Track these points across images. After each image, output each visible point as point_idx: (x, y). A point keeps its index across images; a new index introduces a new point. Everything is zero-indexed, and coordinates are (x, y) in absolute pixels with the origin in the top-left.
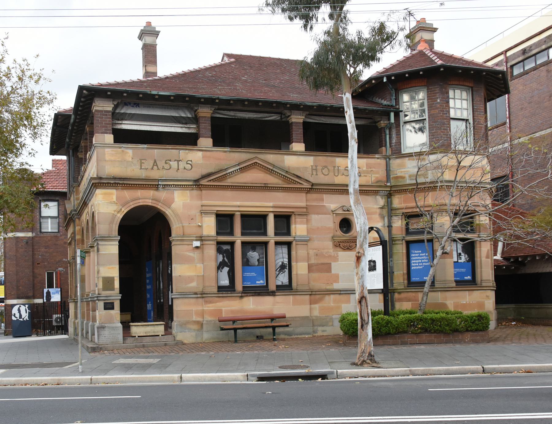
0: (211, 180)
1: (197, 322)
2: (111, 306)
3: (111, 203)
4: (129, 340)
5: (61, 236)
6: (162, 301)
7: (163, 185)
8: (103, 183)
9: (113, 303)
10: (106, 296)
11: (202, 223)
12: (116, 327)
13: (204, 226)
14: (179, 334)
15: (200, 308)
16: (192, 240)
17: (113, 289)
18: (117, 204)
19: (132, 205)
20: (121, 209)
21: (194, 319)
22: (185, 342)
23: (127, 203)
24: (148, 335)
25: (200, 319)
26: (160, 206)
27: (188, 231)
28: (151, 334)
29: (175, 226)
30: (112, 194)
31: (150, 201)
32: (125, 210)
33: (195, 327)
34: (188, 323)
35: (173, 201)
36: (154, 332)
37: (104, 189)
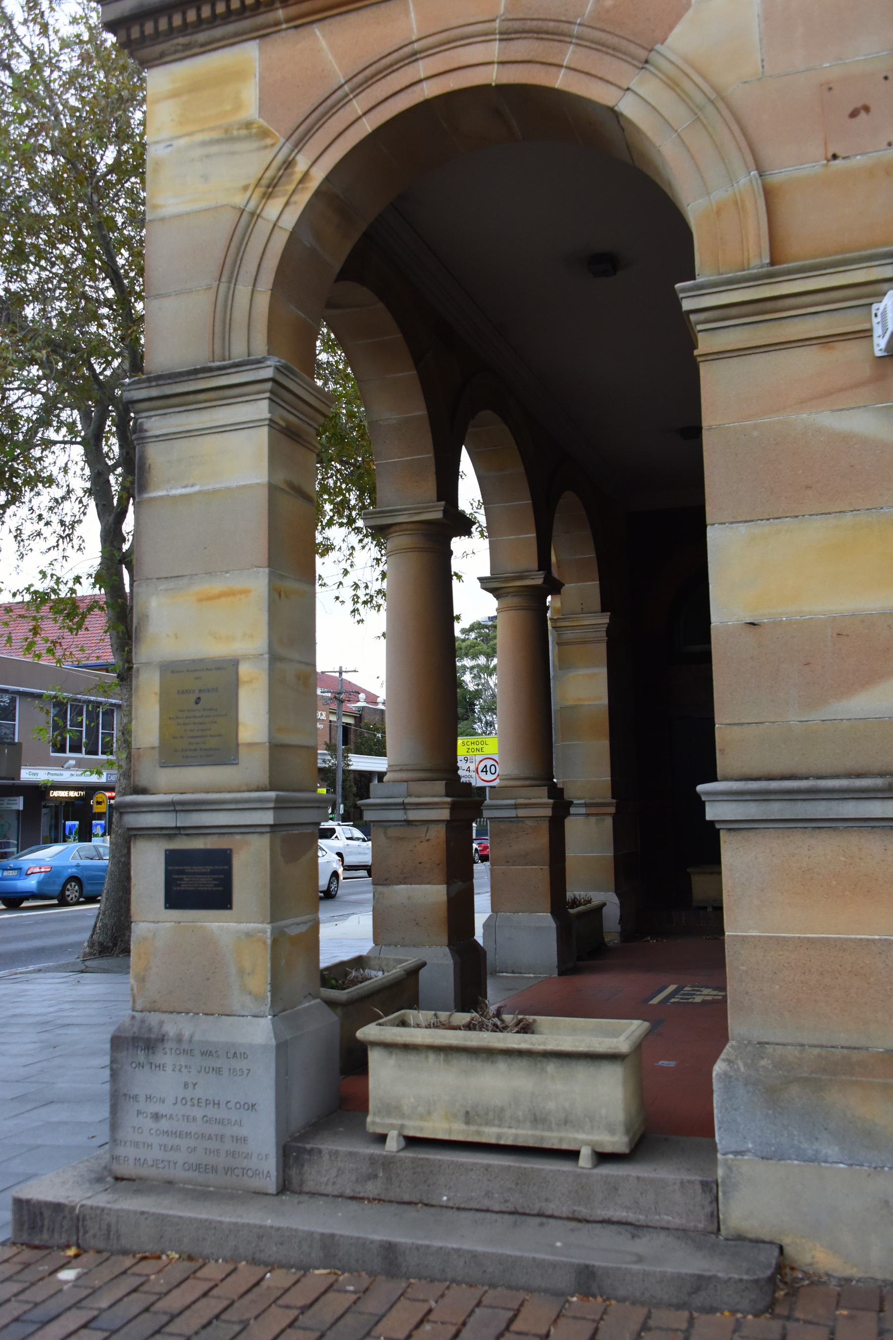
2: (207, 883)
3: (228, 138)
4: (337, 1158)
5: (20, 399)
10: (173, 807)
12: (235, 1053)
17: (225, 752)
19: (363, 117)
20: (289, 164)
22: (817, 1256)
24: (489, 1134)
28: (509, 1135)
30: (238, 75)
32: (316, 167)
36: (538, 1119)
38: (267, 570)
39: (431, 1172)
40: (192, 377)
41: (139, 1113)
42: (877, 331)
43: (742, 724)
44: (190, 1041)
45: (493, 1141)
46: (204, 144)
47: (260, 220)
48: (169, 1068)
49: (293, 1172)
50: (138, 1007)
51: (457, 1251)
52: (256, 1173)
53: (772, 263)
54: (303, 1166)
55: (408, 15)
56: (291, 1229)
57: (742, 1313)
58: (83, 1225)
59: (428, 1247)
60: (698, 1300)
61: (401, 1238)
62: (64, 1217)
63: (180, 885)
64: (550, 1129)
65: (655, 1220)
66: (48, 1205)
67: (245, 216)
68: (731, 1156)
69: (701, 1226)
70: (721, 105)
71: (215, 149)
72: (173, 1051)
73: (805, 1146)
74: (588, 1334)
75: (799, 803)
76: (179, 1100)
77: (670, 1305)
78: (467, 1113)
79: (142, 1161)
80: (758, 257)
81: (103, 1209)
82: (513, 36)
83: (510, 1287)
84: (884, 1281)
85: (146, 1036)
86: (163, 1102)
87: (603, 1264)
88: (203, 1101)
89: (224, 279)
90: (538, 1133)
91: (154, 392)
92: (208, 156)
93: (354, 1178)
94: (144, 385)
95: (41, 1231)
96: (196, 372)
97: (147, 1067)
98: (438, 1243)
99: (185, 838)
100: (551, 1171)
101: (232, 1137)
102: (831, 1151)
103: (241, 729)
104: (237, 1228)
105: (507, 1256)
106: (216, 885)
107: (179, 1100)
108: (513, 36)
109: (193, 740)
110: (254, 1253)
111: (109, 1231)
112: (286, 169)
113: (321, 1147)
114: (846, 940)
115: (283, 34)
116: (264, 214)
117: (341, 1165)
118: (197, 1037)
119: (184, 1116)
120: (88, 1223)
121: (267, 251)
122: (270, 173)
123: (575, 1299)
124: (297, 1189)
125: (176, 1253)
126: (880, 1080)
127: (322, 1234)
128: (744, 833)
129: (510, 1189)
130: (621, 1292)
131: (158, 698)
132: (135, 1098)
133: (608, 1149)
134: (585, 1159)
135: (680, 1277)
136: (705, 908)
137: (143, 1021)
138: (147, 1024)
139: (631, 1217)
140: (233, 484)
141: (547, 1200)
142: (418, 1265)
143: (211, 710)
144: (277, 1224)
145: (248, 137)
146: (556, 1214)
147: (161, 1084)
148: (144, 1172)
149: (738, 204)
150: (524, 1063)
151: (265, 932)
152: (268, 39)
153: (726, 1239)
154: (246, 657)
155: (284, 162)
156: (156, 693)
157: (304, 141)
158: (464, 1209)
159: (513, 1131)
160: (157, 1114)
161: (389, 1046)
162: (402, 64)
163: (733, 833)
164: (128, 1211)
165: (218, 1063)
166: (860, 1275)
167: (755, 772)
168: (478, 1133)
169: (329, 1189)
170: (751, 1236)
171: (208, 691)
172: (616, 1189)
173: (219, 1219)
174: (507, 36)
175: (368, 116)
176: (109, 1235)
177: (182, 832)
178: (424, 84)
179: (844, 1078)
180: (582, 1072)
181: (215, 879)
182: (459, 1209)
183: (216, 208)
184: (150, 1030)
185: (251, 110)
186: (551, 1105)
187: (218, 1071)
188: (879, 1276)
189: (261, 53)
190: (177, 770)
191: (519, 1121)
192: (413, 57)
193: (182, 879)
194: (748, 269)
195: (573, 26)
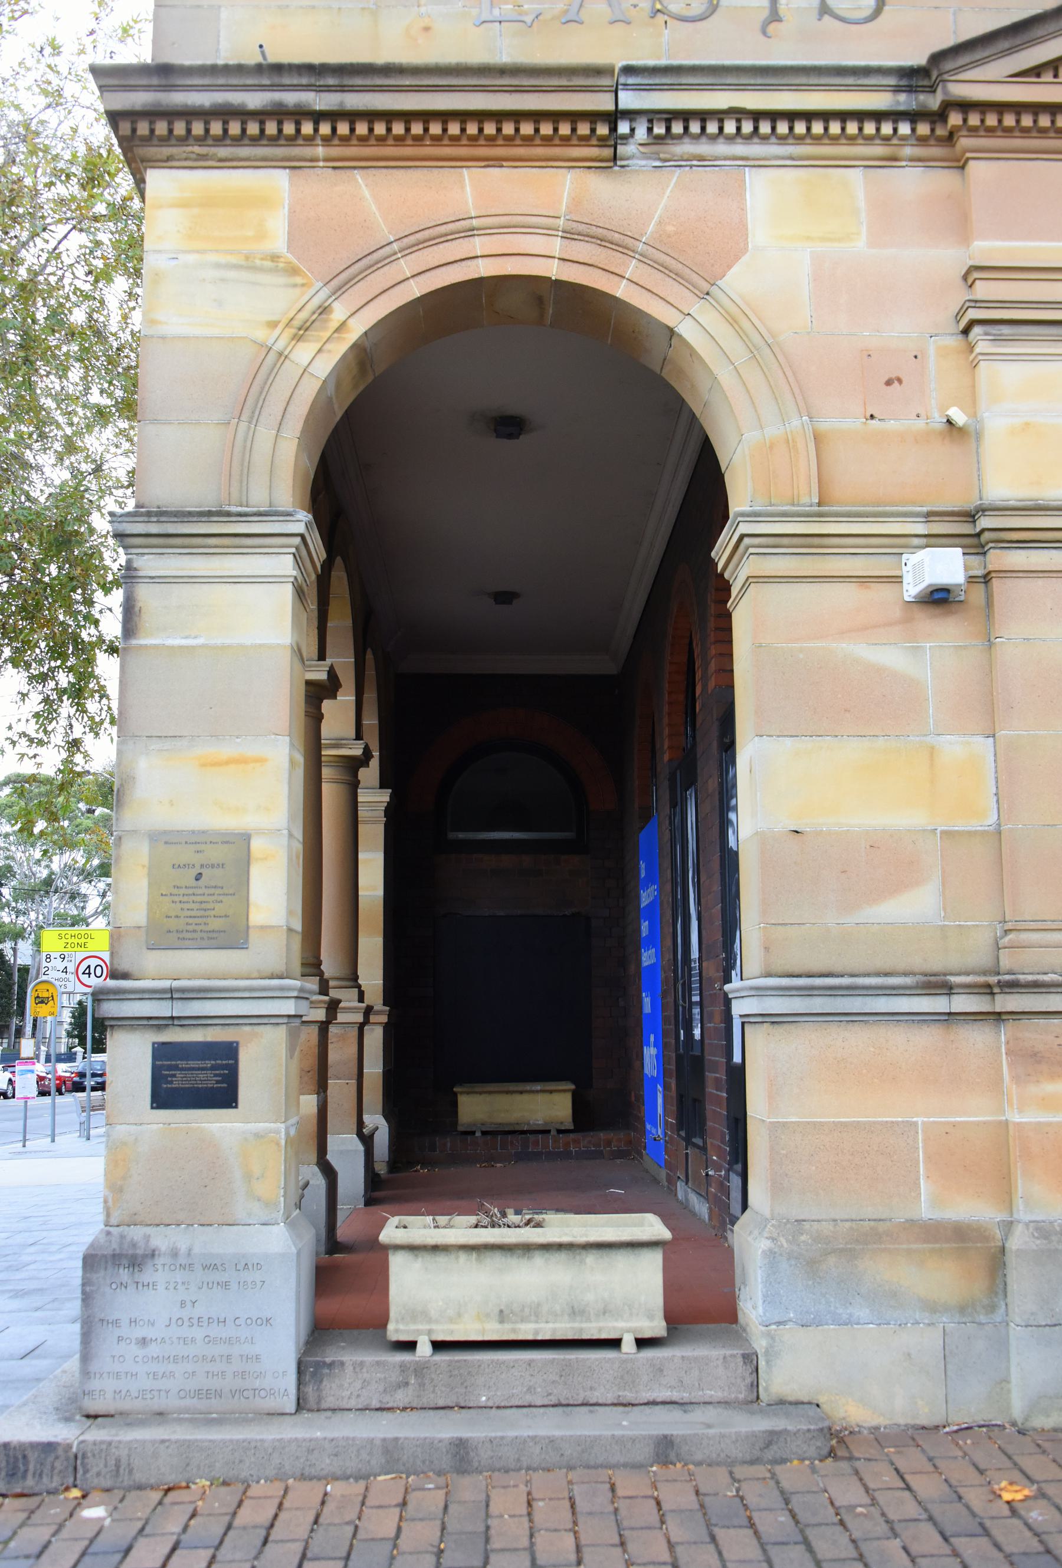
0: (1036, 71)
1: (959, 1237)
2: (207, 1079)
4: (359, 1370)
6: (697, 1032)
7: (652, 116)
8: (189, 114)
9: (229, 1052)
10: (171, 995)
11: (971, 404)
13: (996, 425)
14: (790, 1335)
15: (974, 1112)
16: (901, 543)
17: (234, 936)
18: (294, 271)
19: (412, 281)
20: (324, 310)
21: (925, 1210)
22: (853, 1411)
23: (373, 261)
24: (526, 1332)
25: (972, 1208)
26: (628, 285)
27: (859, 475)
29: (752, 436)
30: (263, 201)
31: (556, 246)
32: (357, 319)
33: (940, 1279)
34: (869, 1238)
35: (734, 246)
36: (576, 1312)
37: (201, 162)
38: (287, 739)
39: (469, 1373)
40: (203, 519)
41: (120, 1339)
42: (907, 579)
43: (786, 924)
44: (189, 1254)
45: (530, 1337)
46: (218, 266)
47: (287, 361)
48: (161, 1287)
49: (310, 1390)
50: (114, 1221)
51: (533, 1438)
52: (271, 1393)
53: (819, 504)
54: (321, 1381)
55: (463, 187)
56: (348, 1438)
57: (809, 1459)
58: (82, 1463)
59: (502, 1438)
60: (769, 1455)
61: (465, 1434)
62: (57, 1458)
63: (171, 1082)
64: (589, 1320)
65: (698, 1395)
66: (34, 1446)
67: (272, 356)
68: (774, 1327)
69: (741, 1396)
70: (776, 350)
71: (232, 274)
72: (167, 1267)
73: (840, 1311)
74: (528, 1563)
75: (839, 999)
76: (174, 1320)
77: (745, 1462)
78: (501, 1311)
79: (123, 1393)
80: (809, 498)
81: (110, 1443)
82: (576, 237)
83: (588, 1467)
84: (906, 1425)
85: (130, 1252)
86: (153, 1325)
87: (681, 1433)
88: (205, 1319)
89: (244, 418)
90: (576, 1325)
91: (154, 529)
92: (223, 280)
93: (381, 1388)
94: (141, 519)
95: (24, 1477)
96: (210, 514)
97: (132, 1288)
98: (511, 1433)
99: (178, 1029)
100: (597, 1360)
101: (242, 1356)
102: (862, 1312)
103: (253, 910)
104: (281, 1446)
105: (586, 1436)
106: (218, 1082)
107: (174, 1320)
108: (576, 237)
109: (190, 921)
110: (303, 1469)
111: (118, 1466)
112: (320, 314)
113: (344, 1359)
114: (874, 1122)
115: (319, 171)
116: (291, 356)
117: (366, 1376)
118: (196, 1250)
119: (179, 1338)
120: (90, 1460)
121: (294, 396)
122: (304, 315)
123: (654, 1469)
124: (315, 1407)
125: (207, 1480)
126: (904, 1246)
127: (384, 1440)
128: (785, 1026)
129: (553, 1382)
130: (699, 1457)
131: (146, 870)
132: (116, 1323)
133: (647, 1334)
134: (628, 1345)
135: (754, 1435)
136: (473, 1133)
137: (122, 1237)
138: (128, 1239)
139: (675, 1396)
140: (248, 642)
141: (591, 1388)
142: (492, 1458)
143: (215, 887)
144: (330, 1435)
145: (275, 271)
146: (600, 1401)
147: (150, 1306)
148: (126, 1405)
149: (789, 442)
150: (562, 1256)
151: (278, 1132)
152: (297, 171)
153: (769, 1405)
154: (260, 832)
155: (320, 307)
156: (144, 866)
157: (343, 289)
158: (505, 1407)
159: (551, 1325)
160: (144, 1339)
161: (412, 1248)
162: (457, 236)
163: (776, 1026)
164: (144, 1442)
165: (223, 1277)
166: (887, 1422)
167: (797, 970)
168: (514, 1331)
169: (352, 1403)
170: (791, 1398)
171: (213, 866)
172: (661, 1371)
173: (258, 1437)
174: (569, 235)
175: (417, 279)
176: (118, 1471)
177: (176, 1022)
178: (480, 260)
179: (875, 1246)
180: (622, 1260)
181: (216, 1075)
182: (498, 1407)
183: (232, 339)
184: (134, 1245)
185: (278, 240)
186: (590, 1297)
187: (225, 1285)
188: (902, 1421)
189: (291, 184)
190: (170, 953)
191: (556, 1315)
192: (471, 232)
193: (174, 1076)
194: (798, 505)
195: (637, 243)
